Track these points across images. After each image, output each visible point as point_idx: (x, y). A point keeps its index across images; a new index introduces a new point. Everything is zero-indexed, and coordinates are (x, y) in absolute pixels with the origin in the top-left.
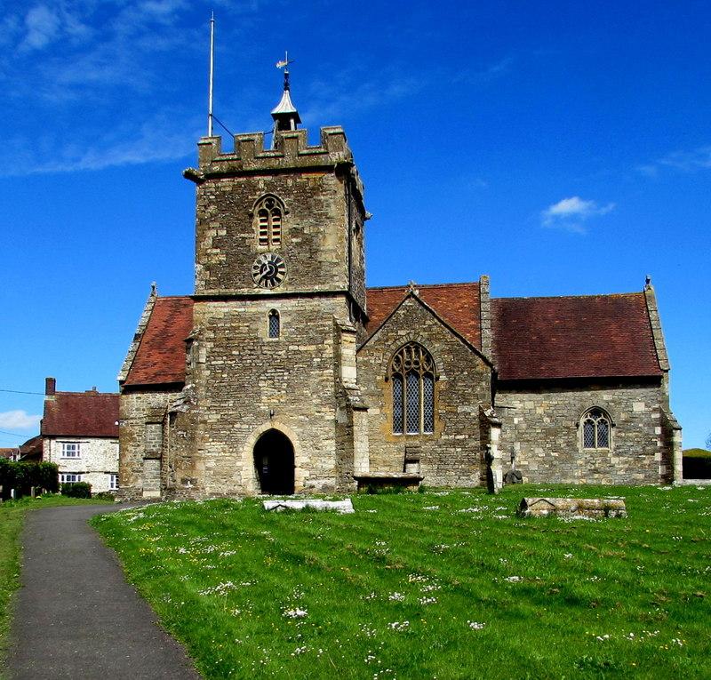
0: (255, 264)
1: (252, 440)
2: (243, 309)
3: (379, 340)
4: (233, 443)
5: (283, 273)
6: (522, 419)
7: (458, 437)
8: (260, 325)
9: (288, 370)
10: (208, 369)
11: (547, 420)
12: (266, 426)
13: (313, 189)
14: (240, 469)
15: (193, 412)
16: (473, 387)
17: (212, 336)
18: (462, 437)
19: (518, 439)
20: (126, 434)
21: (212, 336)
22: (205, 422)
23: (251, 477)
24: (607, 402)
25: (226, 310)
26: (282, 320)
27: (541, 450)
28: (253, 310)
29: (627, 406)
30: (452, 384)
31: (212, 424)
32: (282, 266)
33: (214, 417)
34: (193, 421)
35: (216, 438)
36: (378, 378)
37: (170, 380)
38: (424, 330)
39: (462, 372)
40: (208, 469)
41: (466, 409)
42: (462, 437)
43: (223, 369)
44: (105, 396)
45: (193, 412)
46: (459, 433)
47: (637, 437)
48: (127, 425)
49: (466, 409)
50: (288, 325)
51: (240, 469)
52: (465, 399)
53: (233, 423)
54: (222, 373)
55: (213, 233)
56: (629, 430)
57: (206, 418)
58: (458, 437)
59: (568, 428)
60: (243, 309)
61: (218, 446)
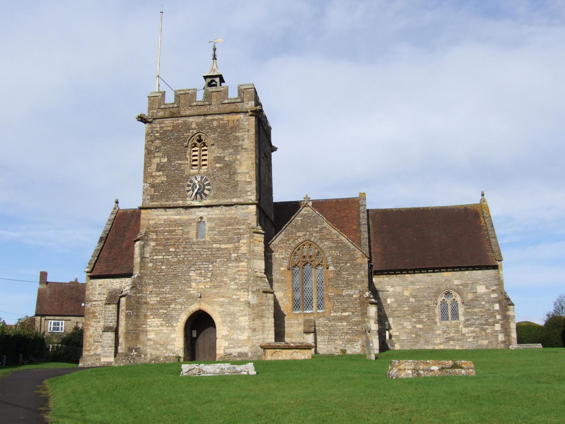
1: (184, 318)
2: (178, 217)
3: (282, 240)
4: (169, 319)
6: (393, 300)
10: (151, 262)
11: (412, 300)
12: (194, 308)
13: (231, 128)
15: (138, 295)
16: (355, 275)
17: (155, 237)
20: (90, 313)
21: (155, 237)
24: (457, 285)
25: (166, 217)
26: (208, 225)
27: (409, 323)
28: (186, 217)
29: (472, 289)
30: (338, 273)
31: (153, 305)
36: (282, 269)
38: (317, 232)
39: (346, 264)
41: (350, 292)
43: (162, 262)
45: (138, 295)
46: (344, 310)
47: (481, 312)
49: (350, 292)
51: (174, 340)
52: (348, 284)
53: (169, 304)
54: (162, 265)
55: (157, 160)
59: (428, 306)
60: (178, 217)
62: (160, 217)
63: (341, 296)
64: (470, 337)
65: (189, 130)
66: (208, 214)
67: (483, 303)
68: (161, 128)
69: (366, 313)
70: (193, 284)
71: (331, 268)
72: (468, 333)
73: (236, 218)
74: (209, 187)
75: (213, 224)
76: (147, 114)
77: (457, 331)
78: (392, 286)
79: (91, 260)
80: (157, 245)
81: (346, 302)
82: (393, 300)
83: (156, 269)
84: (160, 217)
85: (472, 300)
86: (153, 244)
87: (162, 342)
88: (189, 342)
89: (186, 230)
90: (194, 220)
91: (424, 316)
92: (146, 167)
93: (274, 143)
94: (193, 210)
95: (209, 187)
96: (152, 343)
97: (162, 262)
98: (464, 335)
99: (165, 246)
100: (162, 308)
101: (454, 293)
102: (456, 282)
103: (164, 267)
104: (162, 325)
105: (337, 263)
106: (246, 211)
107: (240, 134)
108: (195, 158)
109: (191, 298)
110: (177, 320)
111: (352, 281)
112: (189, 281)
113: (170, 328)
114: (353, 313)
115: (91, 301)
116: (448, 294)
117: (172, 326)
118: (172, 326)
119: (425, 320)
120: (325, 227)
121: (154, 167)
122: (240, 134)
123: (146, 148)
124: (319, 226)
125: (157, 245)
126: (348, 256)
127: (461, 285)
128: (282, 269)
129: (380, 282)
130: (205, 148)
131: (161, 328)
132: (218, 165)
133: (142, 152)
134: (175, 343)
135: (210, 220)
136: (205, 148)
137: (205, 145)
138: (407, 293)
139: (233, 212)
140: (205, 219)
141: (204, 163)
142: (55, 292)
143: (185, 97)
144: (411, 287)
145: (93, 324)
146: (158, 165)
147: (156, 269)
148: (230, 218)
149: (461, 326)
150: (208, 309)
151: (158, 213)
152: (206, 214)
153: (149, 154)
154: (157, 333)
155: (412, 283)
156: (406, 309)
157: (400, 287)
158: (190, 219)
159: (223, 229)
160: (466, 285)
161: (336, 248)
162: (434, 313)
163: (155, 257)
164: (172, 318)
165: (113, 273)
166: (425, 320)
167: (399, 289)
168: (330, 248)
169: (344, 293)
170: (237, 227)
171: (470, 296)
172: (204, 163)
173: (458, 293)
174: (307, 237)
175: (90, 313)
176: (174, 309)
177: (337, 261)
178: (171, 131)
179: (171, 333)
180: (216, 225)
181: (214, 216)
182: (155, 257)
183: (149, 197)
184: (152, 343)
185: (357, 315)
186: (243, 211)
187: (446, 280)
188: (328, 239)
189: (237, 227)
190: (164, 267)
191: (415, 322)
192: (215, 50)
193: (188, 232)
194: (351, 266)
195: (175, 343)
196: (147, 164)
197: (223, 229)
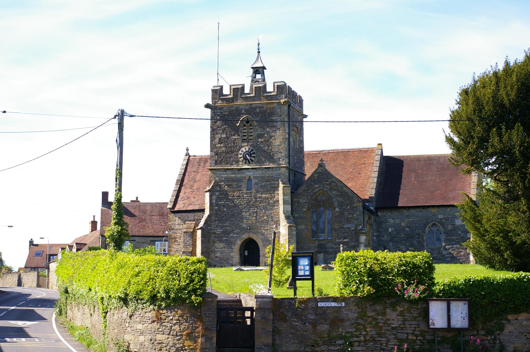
0: (241, 152)
1: (239, 243)
2: (234, 176)
3: (304, 190)
4: (229, 244)
5: (254, 157)
6: (393, 229)
7: (345, 240)
8: (242, 184)
9: (257, 207)
10: (216, 206)
11: (407, 229)
12: (245, 236)
13: (269, 113)
14: (232, 257)
15: (209, 228)
16: (353, 214)
17: (219, 189)
18: (346, 240)
19: (391, 241)
20: (172, 238)
21: (219, 189)
22: (215, 233)
23: (238, 261)
24: (441, 219)
25: (226, 176)
26: (254, 181)
27: (404, 247)
28: (239, 176)
29: (452, 222)
30: (341, 213)
31: (218, 234)
32: (254, 153)
33: (219, 231)
34: (209, 233)
35: (221, 241)
36: (304, 210)
37: (197, 208)
38: (328, 185)
39: (347, 206)
40: (217, 257)
41: (349, 226)
42: (346, 240)
43: (224, 206)
44: (145, 204)
45: (209, 228)
46: (345, 238)
47: (457, 239)
48: (173, 233)
49: (349, 226)
50: (256, 184)
51: (232, 257)
52: (348, 220)
53: (229, 234)
54: (224, 208)
55: (220, 135)
56: (453, 235)
57: (216, 231)
58: (345, 240)
59: (419, 234)
60: (234, 176)
61: (221, 245)
62: (222, 175)
63: (343, 228)
64: (448, 257)
65: (240, 114)
66: (254, 174)
67: (459, 232)
68: (221, 112)
69: (358, 240)
70: (245, 221)
71: (337, 209)
72: (447, 254)
73: (272, 177)
74: (254, 155)
75: (257, 181)
76: (211, 103)
77: (439, 253)
78: (393, 219)
79: (171, 199)
80: (220, 194)
81: (347, 232)
82: (393, 229)
83: (220, 210)
84: (222, 175)
85: (451, 230)
86: (217, 193)
87: (225, 259)
88: (242, 258)
89: (240, 184)
90: (245, 177)
91: (415, 241)
92: (212, 141)
93: (305, 113)
94: (244, 171)
95: (254, 155)
96: (218, 259)
97: (224, 206)
98: (444, 256)
99: (226, 195)
100: (224, 237)
101: (439, 225)
102: (440, 217)
103: (225, 209)
104: (224, 247)
105: (341, 206)
106: (279, 172)
107: (275, 118)
108: (244, 134)
109: (244, 230)
110: (234, 244)
111: (351, 218)
112: (242, 218)
113: (230, 250)
114: (351, 239)
115: (172, 229)
116: (434, 225)
117: (231, 248)
118: (231, 248)
119: (416, 244)
120: (333, 181)
121: (217, 140)
122: (275, 118)
123: (211, 127)
124: (330, 181)
125: (220, 194)
126: (348, 201)
127: (444, 219)
128: (304, 210)
129: (384, 216)
130: (251, 127)
131: (224, 249)
132: (260, 140)
133: (209, 130)
134: (233, 259)
135: (255, 178)
136: (251, 127)
137: (251, 125)
138: (403, 224)
139: (270, 172)
140: (252, 177)
141: (251, 138)
142: (455, 282)
143: (238, 91)
144: (406, 220)
145: (174, 246)
146: (220, 139)
147: (220, 210)
148: (269, 177)
149: (442, 249)
150: (254, 237)
151: (220, 173)
152: (252, 173)
153: (214, 131)
154: (221, 253)
155: (408, 217)
156: (403, 236)
157: (399, 220)
158: (242, 177)
159: (264, 184)
160: (446, 219)
161: (341, 196)
162: (423, 239)
163: (219, 203)
164: (231, 243)
165: (188, 209)
166: (416, 244)
167: (397, 221)
168: (336, 195)
169: (345, 226)
170: (273, 182)
171: (450, 227)
172: (251, 138)
173: (441, 225)
174: (321, 188)
175: (172, 238)
176: (232, 237)
177: (341, 205)
178: (228, 115)
179: (230, 253)
180: (259, 181)
181: (258, 175)
182: (219, 203)
183: (214, 162)
184: (218, 259)
185: (354, 241)
186: (277, 172)
187: (433, 215)
188: (335, 190)
189: (273, 182)
190: (225, 209)
191: (409, 246)
192: (259, 44)
193: (241, 186)
194: (350, 208)
195: (233, 259)
196: (212, 139)
197: (264, 184)
